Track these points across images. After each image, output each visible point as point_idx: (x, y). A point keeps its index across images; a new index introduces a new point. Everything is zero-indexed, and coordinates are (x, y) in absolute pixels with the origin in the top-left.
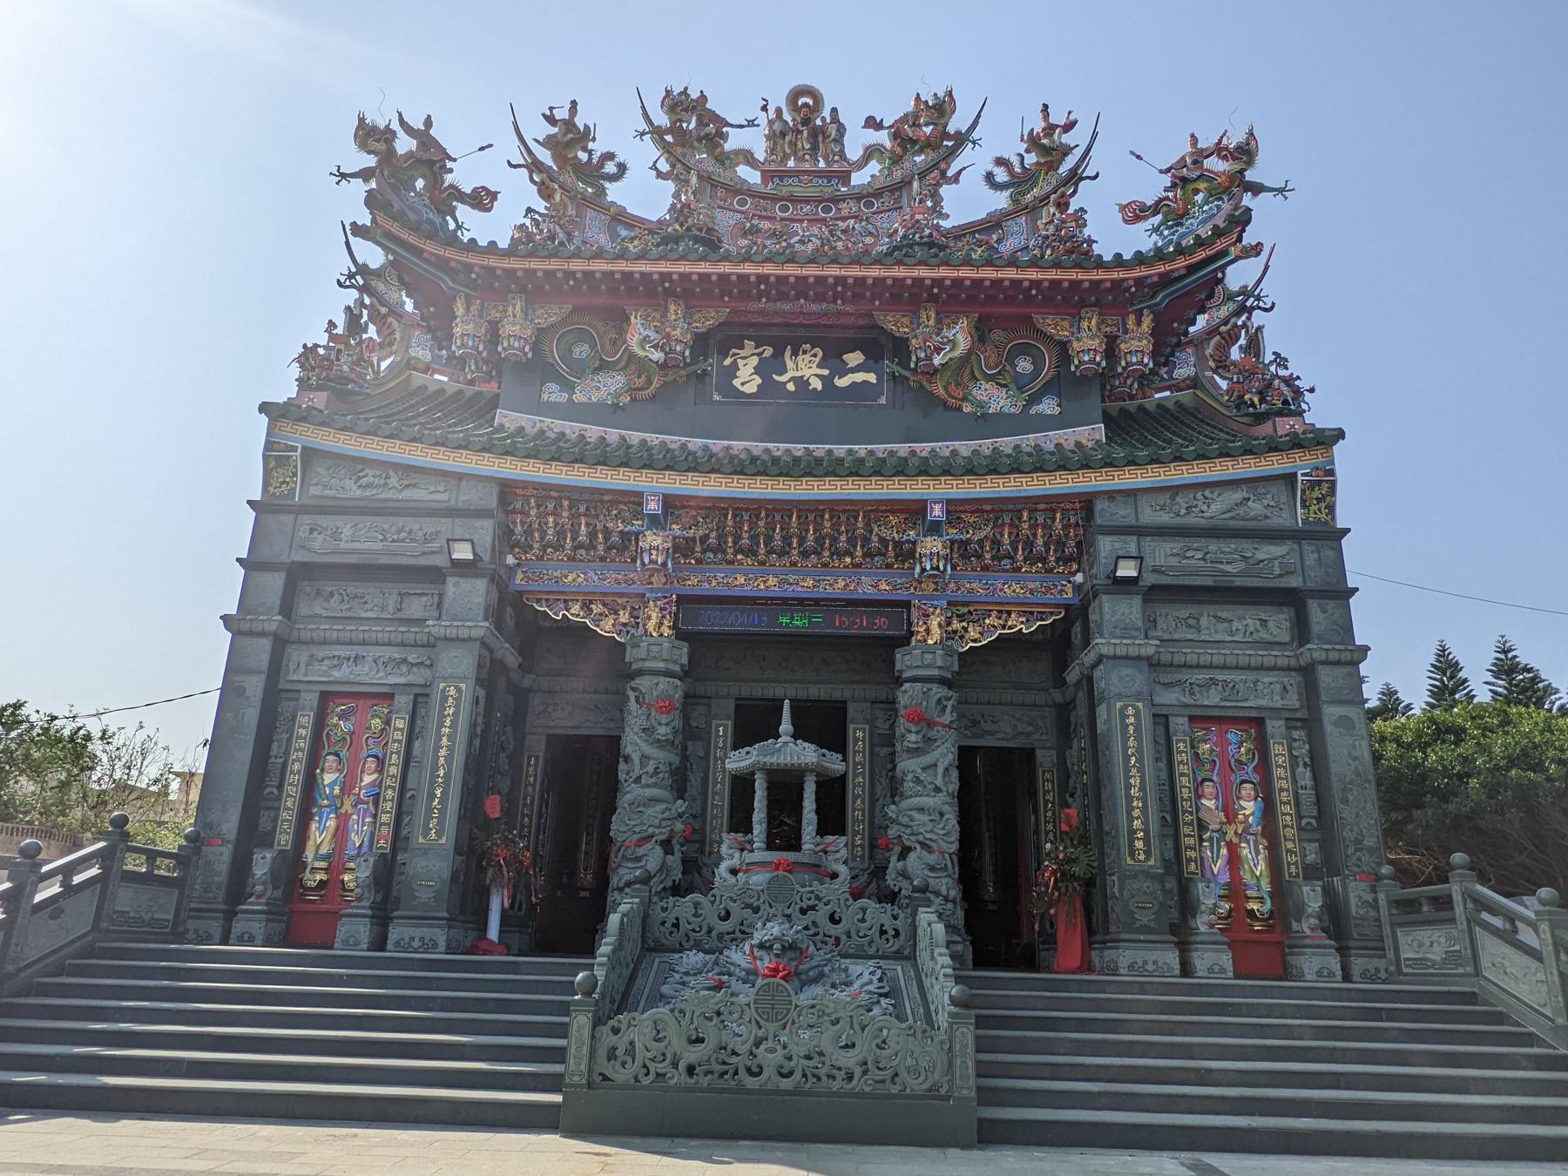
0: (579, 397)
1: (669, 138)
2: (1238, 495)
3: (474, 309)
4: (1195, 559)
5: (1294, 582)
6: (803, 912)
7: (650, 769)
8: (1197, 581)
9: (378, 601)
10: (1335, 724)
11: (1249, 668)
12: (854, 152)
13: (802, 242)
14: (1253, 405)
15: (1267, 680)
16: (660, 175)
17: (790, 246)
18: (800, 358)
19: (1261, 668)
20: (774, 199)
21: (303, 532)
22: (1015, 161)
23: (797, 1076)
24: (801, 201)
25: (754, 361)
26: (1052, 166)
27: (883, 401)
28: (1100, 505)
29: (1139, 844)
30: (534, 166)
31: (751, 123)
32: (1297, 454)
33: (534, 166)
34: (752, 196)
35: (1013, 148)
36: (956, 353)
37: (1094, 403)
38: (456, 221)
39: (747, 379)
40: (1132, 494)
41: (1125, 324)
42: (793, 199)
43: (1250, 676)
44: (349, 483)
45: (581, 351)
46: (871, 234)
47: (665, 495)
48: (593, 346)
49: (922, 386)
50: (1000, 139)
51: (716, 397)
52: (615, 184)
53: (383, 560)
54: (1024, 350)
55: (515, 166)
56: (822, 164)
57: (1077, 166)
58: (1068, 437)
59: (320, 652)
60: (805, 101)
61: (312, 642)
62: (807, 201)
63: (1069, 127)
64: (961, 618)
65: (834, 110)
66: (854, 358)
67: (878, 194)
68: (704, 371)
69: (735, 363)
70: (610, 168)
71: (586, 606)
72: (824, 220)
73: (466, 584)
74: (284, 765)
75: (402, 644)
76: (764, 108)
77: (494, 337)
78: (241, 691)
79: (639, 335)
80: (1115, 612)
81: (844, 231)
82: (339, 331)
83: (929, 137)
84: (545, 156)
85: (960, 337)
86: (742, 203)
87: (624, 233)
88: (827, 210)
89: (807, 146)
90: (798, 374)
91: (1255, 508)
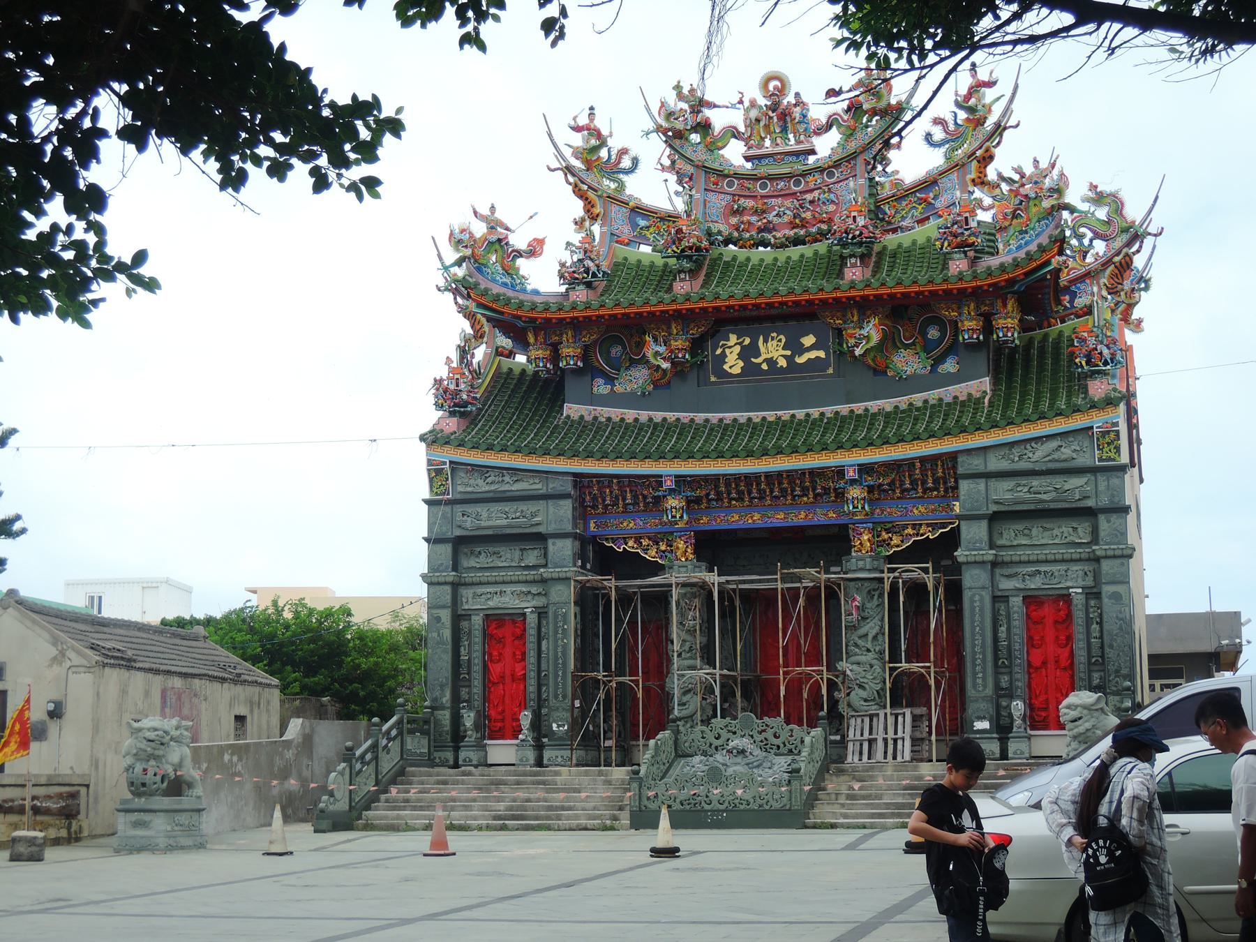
0: (619, 388)
2: (1054, 444)
4: (1023, 494)
5: (1090, 503)
6: (760, 733)
7: (687, 648)
8: (1025, 507)
9: (509, 556)
10: (1110, 597)
11: (1063, 561)
13: (777, 215)
14: (1082, 366)
15: (1075, 568)
17: (769, 222)
19: (1072, 560)
21: (459, 517)
22: (949, 118)
23: (726, 804)
25: (737, 349)
26: (980, 122)
27: (831, 371)
29: (979, 681)
30: (568, 170)
32: (1094, 413)
33: (568, 170)
34: (738, 179)
36: (872, 344)
39: (733, 364)
40: (984, 449)
42: (772, 178)
43: (1063, 567)
44: (480, 482)
45: (616, 351)
46: (833, 202)
47: (676, 476)
48: (624, 348)
51: (713, 379)
52: (632, 176)
53: (508, 531)
55: (553, 170)
57: (1004, 114)
58: (961, 390)
59: (480, 590)
60: (775, 85)
61: (473, 584)
63: (990, 84)
64: (888, 531)
65: (797, 95)
66: (809, 340)
67: (837, 164)
68: (702, 362)
69: (724, 352)
71: (638, 540)
73: (560, 543)
74: (469, 660)
75: (526, 582)
76: (741, 102)
78: (438, 619)
79: (654, 349)
80: (973, 533)
81: (811, 202)
82: (454, 365)
84: (577, 164)
86: (730, 185)
87: (642, 223)
88: (797, 183)
90: (769, 356)
91: (1066, 452)
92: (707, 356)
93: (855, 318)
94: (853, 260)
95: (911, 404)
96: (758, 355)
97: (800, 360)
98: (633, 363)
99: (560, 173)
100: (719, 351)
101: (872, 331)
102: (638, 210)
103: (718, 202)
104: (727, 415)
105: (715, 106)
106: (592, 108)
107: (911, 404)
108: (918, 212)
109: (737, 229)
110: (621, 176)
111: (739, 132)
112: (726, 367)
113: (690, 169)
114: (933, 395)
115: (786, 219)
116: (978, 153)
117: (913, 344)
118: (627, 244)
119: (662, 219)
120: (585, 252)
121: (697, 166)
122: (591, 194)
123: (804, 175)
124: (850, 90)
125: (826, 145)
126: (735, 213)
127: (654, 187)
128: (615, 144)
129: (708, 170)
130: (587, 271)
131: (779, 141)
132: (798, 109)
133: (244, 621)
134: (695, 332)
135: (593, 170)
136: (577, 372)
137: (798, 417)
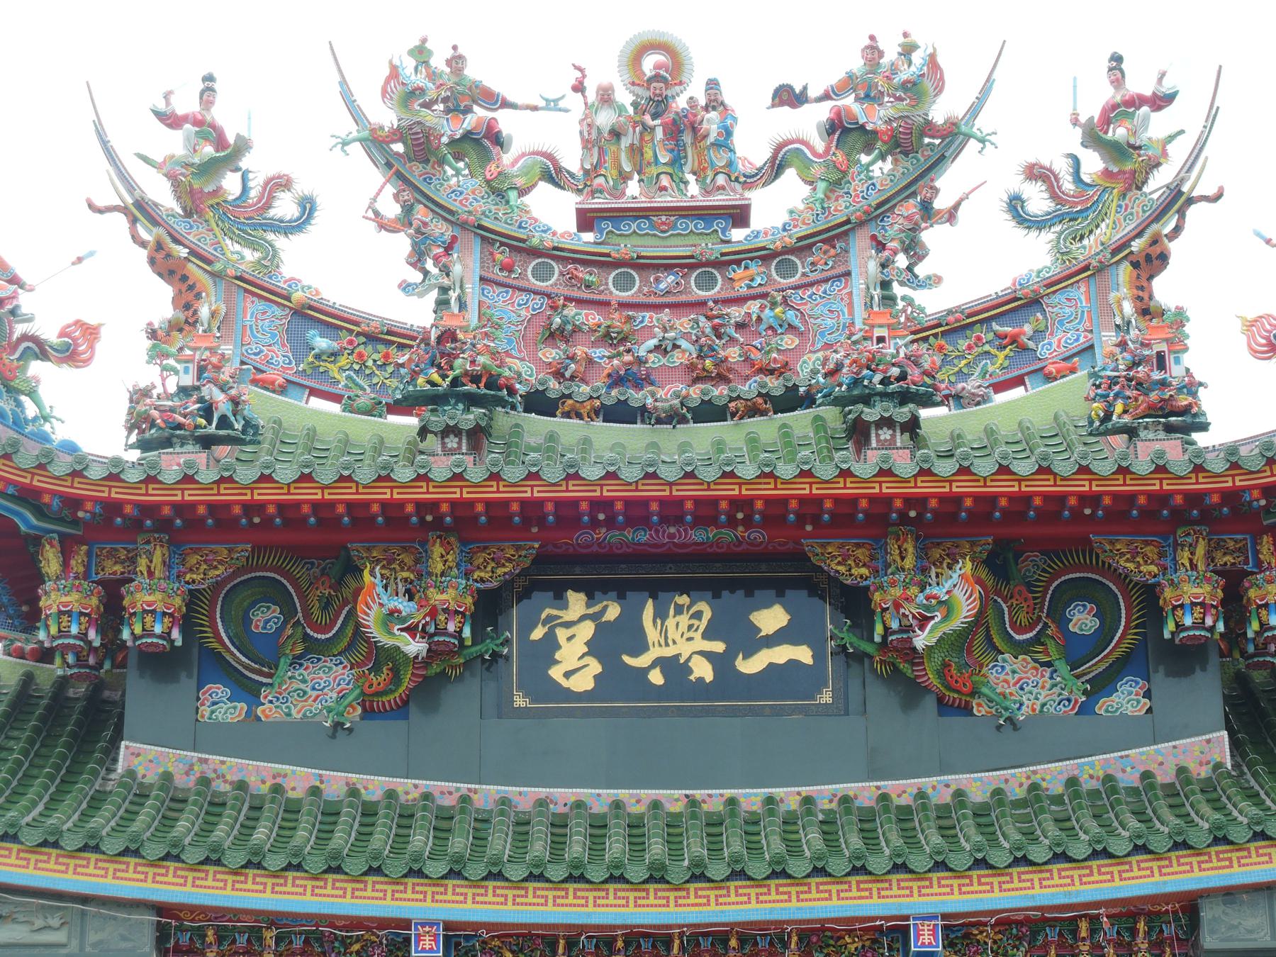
1: (399, 148)
3: (77, 564)
12: (752, 148)
16: (384, 225)
17: (640, 361)
18: (670, 622)
20: (604, 263)
22: (1062, 168)
24: (657, 267)
25: (587, 630)
26: (1135, 182)
27: (826, 697)
28: (1208, 913)
30: (140, 211)
31: (552, 105)
33: (140, 211)
35: (1059, 145)
37: (1206, 690)
38: (38, 403)
39: (575, 665)
41: (1257, 552)
42: (643, 265)
45: (265, 618)
46: (791, 328)
47: (448, 926)
49: (896, 669)
50: (1025, 128)
51: (520, 701)
52: (296, 239)
54: (1083, 591)
56: (694, 189)
58: (1163, 758)
60: (658, 69)
62: (667, 265)
63: (1160, 101)
65: (712, 85)
66: (771, 619)
67: (803, 247)
68: (495, 655)
70: (285, 207)
72: (702, 304)
76: (579, 88)
77: (112, 611)
79: (385, 609)
81: (740, 326)
83: (893, 138)
85: (959, 595)
87: (322, 343)
89: (664, 158)
90: (668, 652)
92: (507, 642)
93: (909, 562)
94: (885, 434)
95: (1034, 787)
96: (640, 646)
97: (750, 666)
98: (313, 650)
99: (121, 220)
100: (538, 633)
101: (957, 591)
102: (309, 314)
103: (514, 310)
104: (557, 792)
105: (513, 106)
106: (209, 78)
107: (1034, 787)
108: (998, 364)
109: (558, 375)
110: (270, 236)
111: (559, 169)
112: (556, 673)
113: (441, 229)
114: (1091, 768)
115: (677, 359)
116: (1136, 245)
117: (1037, 640)
118: (282, 390)
119: (372, 338)
120: (201, 370)
121: (463, 226)
122: (194, 270)
123: (721, 264)
124: (826, 96)
125: (776, 208)
126: (554, 336)
127: (358, 262)
128: (259, 165)
129: (488, 237)
130: (207, 411)
131: (665, 181)
132: (713, 115)
133: (278, 267)
134: (491, 575)
135: (203, 218)
136: (161, 663)
137: (745, 805)
